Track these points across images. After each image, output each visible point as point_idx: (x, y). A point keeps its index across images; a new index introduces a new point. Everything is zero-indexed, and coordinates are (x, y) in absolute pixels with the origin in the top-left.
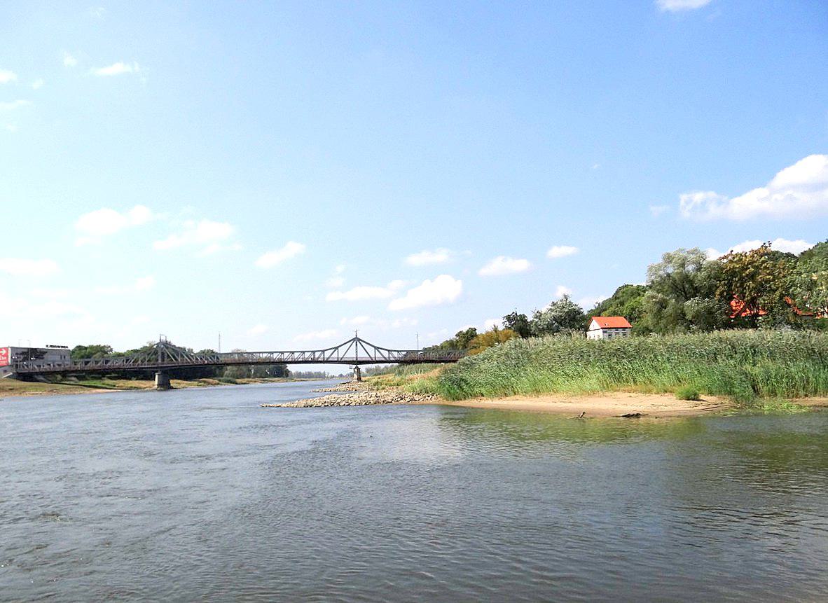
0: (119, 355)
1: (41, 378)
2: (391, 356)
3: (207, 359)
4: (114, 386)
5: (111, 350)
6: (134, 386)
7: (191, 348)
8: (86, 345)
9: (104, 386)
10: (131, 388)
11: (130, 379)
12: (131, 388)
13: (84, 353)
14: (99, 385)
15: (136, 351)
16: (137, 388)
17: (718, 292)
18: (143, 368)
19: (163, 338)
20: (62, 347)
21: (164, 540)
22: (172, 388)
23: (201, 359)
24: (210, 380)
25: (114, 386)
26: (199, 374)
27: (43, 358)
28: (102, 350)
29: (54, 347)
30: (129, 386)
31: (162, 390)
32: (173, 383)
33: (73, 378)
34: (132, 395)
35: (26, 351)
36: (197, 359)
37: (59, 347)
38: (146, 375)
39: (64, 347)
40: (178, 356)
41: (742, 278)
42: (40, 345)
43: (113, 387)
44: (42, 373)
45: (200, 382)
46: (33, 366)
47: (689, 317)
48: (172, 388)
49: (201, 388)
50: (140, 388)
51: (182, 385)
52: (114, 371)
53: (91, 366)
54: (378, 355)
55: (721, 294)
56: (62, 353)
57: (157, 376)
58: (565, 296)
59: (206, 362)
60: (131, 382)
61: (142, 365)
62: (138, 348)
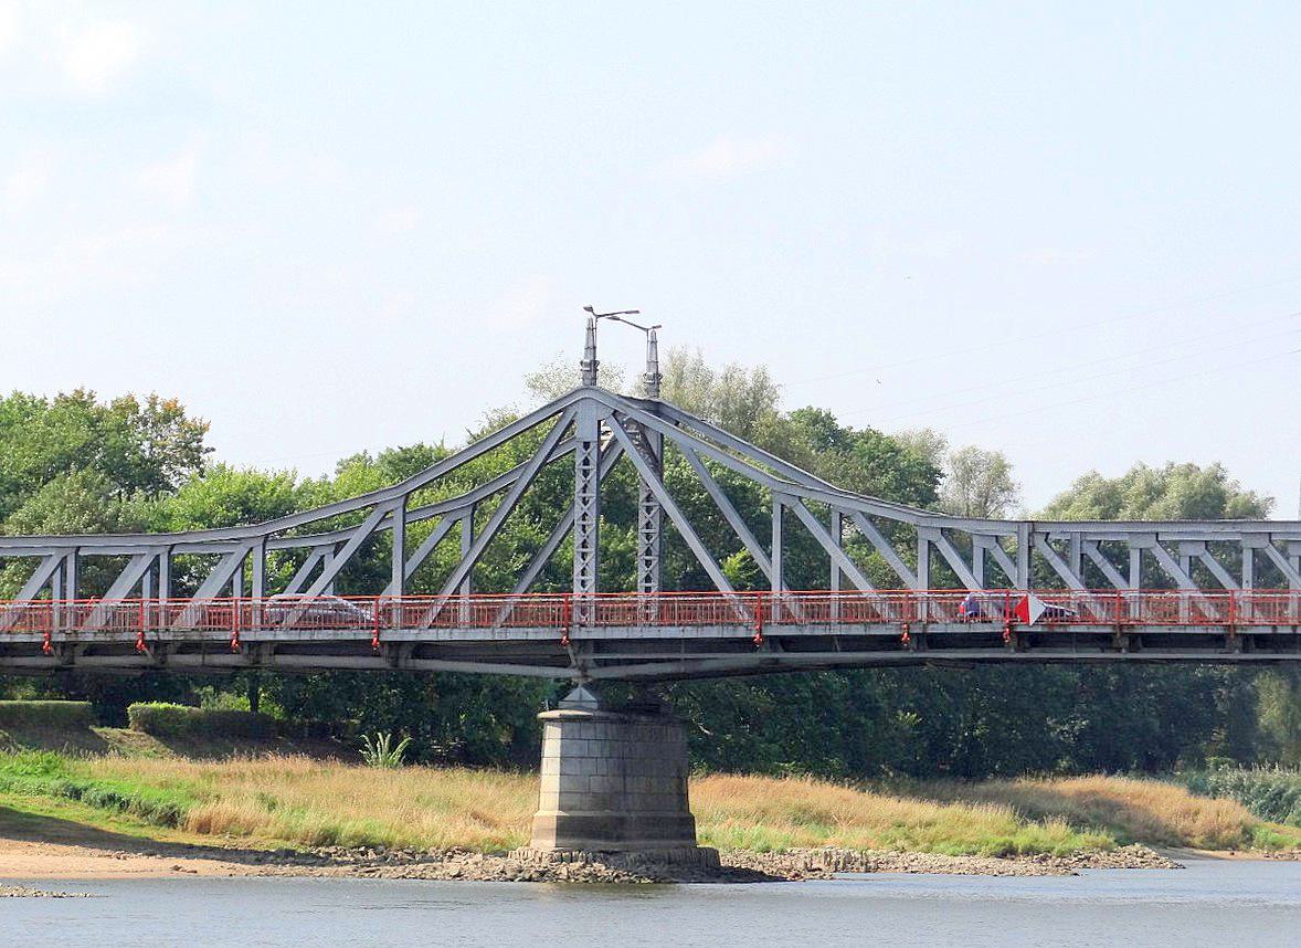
0: (256, 507)
3: (1043, 577)
4: (171, 819)
5: (191, 452)
6: (352, 823)
7: (122, 395)
9: (74, 812)
10: (320, 850)
11: (352, 754)
12: (320, 850)
14: (34, 805)
15: (412, 464)
16: (372, 851)
18: (421, 649)
22: (708, 868)
23: (1094, 579)
24: (1163, 798)
25: (171, 819)
26: (1062, 729)
30: (313, 822)
31: (593, 884)
32: (727, 810)
34: (647, 902)
36: (1161, 583)
38: (456, 715)
40: (967, 559)
43: (161, 833)
45: (1034, 814)
47: (117, 805)
48: (708, 868)
49: (1023, 879)
50: (413, 855)
51: (843, 840)
52: (252, 665)
57: (552, 743)
59: (1036, 608)
60: (339, 775)
61: (412, 617)
62: (450, 433)
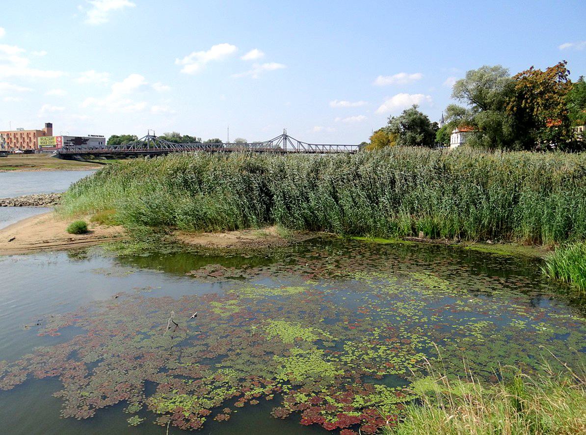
1: (79, 157)
2: (324, 149)
8: (227, 138)
13: (116, 141)
17: (509, 108)
19: (152, 134)
20: (100, 136)
21: (534, 386)
27: (86, 144)
28: (130, 139)
29: (94, 136)
33: (104, 158)
35: (74, 138)
36: (165, 147)
37: (97, 136)
39: (101, 136)
41: (532, 94)
42: (83, 134)
44: (81, 155)
46: (74, 149)
53: (118, 150)
54: (301, 147)
55: (512, 109)
56: (100, 140)
58: (414, 106)
